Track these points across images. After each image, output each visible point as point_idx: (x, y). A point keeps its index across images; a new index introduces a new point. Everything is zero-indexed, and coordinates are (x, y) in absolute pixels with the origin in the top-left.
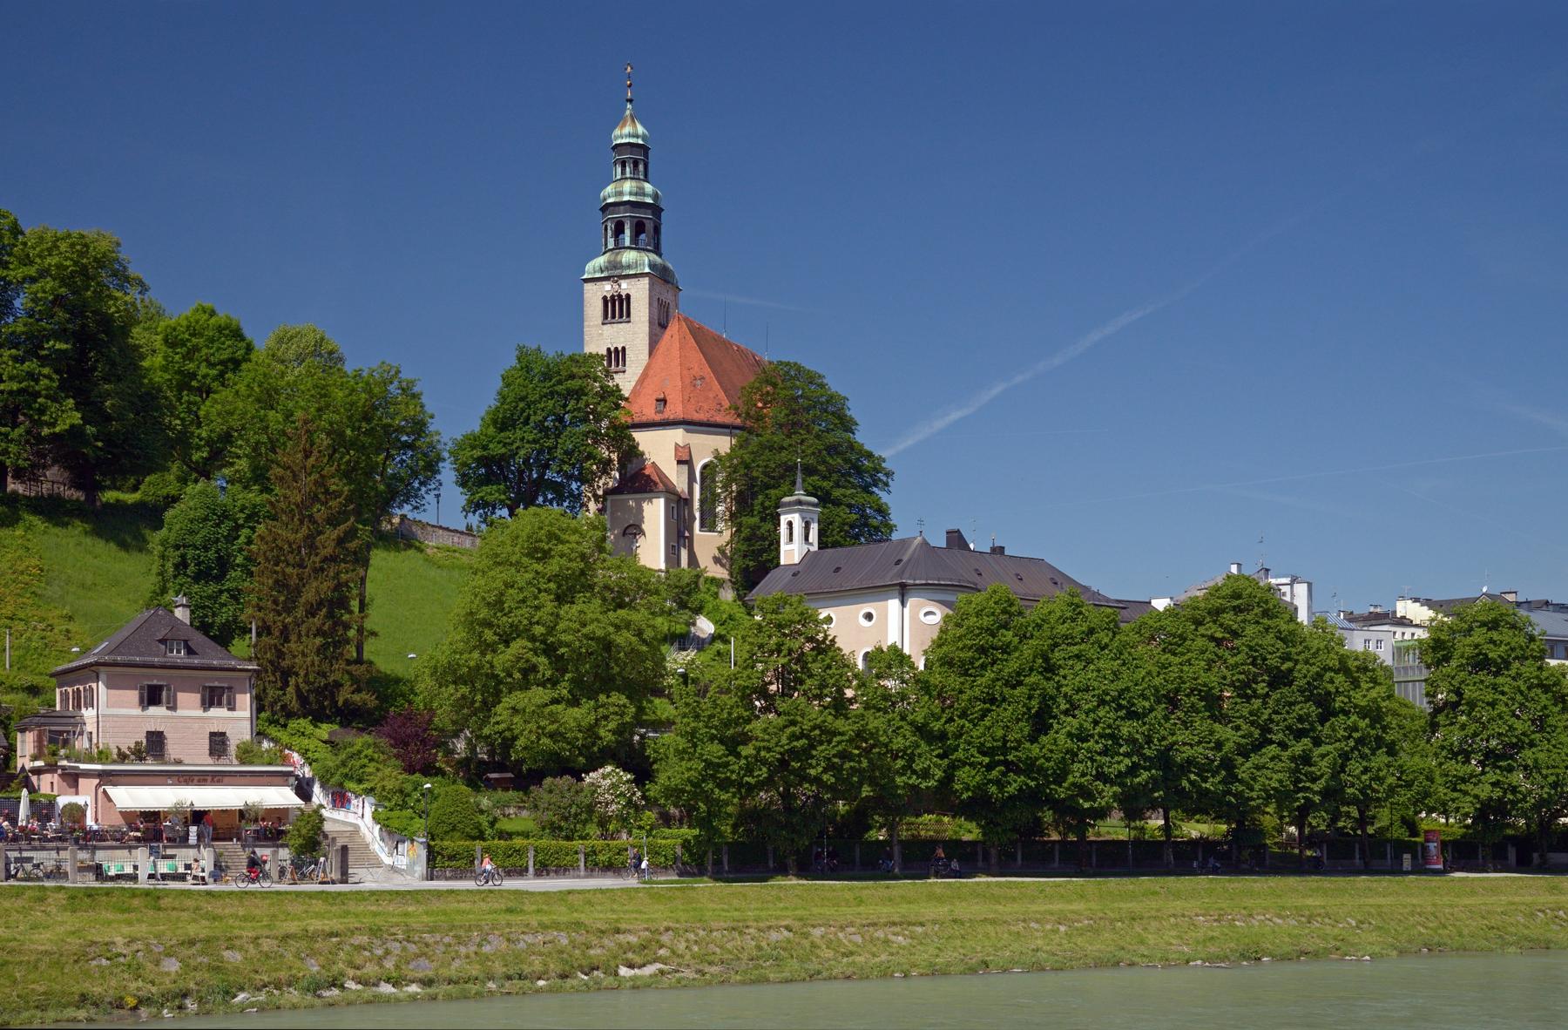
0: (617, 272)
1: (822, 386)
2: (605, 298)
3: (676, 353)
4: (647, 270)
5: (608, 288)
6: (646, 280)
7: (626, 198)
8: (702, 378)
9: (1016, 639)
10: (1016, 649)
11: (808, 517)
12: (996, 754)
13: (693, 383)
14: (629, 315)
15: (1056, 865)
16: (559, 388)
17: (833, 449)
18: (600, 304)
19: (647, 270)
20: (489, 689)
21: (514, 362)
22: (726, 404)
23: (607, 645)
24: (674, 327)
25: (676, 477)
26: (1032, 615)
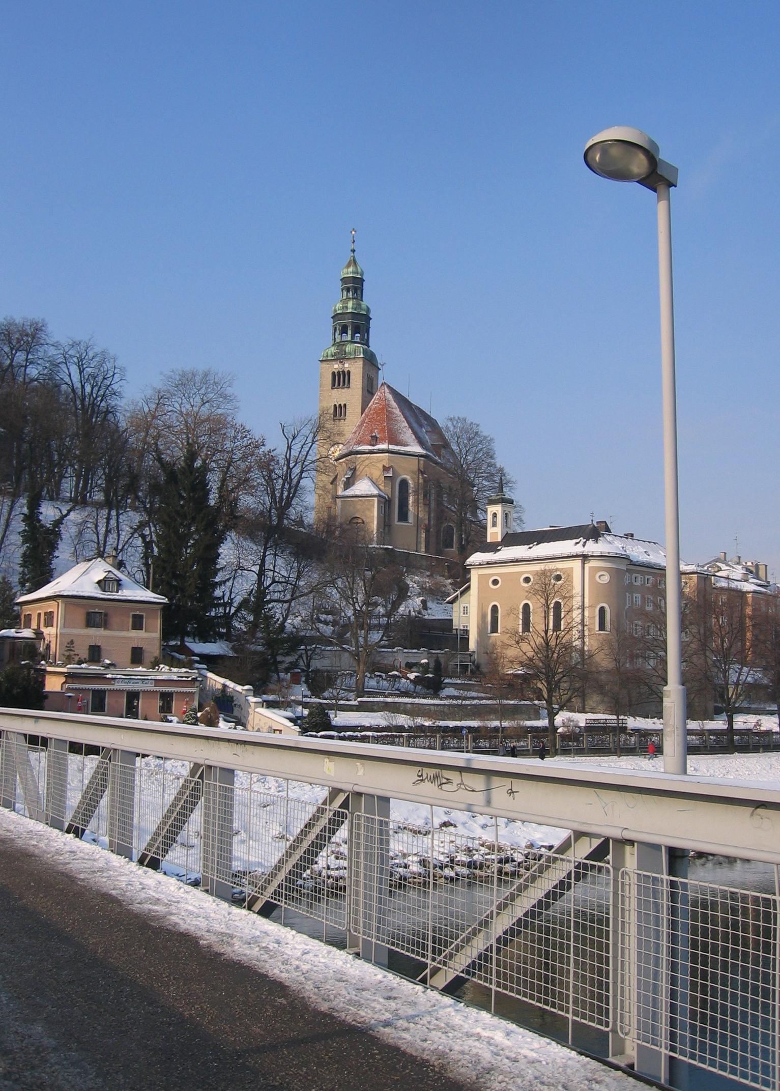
2: (333, 373)
5: (336, 366)
18: (330, 377)
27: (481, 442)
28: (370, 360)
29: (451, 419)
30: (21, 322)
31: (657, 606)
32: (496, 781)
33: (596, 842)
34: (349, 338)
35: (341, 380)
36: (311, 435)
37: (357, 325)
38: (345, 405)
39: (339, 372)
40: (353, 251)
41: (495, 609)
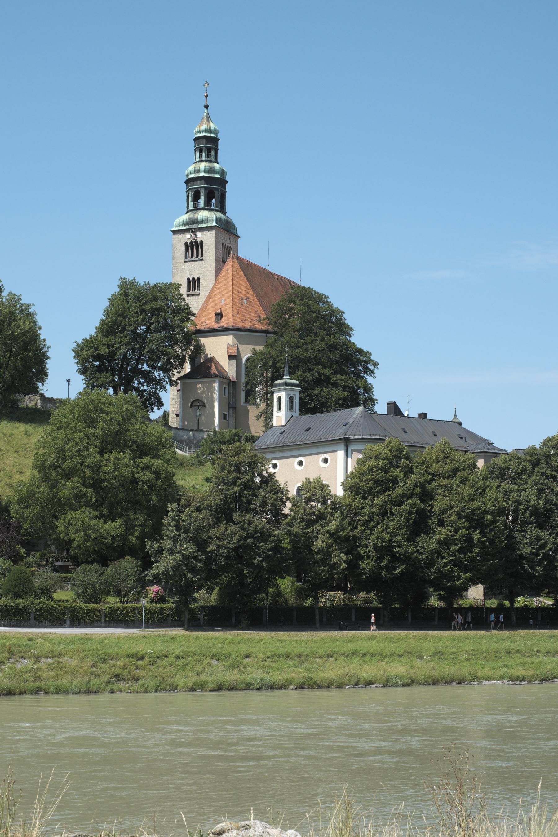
0: (195, 226)
1: (329, 304)
2: (186, 244)
3: (230, 281)
4: (214, 224)
5: (188, 237)
6: (213, 233)
7: (202, 174)
8: (247, 299)
9: (402, 475)
10: (401, 480)
11: (292, 394)
12: (385, 550)
13: (239, 304)
14: (202, 256)
15: (436, 622)
16: (147, 307)
17: (332, 347)
18: (182, 248)
19: (214, 224)
20: (56, 507)
21: (117, 290)
22: (264, 315)
23: (134, 481)
24: (229, 263)
25: (229, 368)
26: (417, 457)
28: (226, 229)
30: (182, 458)
31: (542, 596)
33: (206, 689)
35: (194, 250)
37: (211, 191)
38: (198, 278)
39: (191, 243)
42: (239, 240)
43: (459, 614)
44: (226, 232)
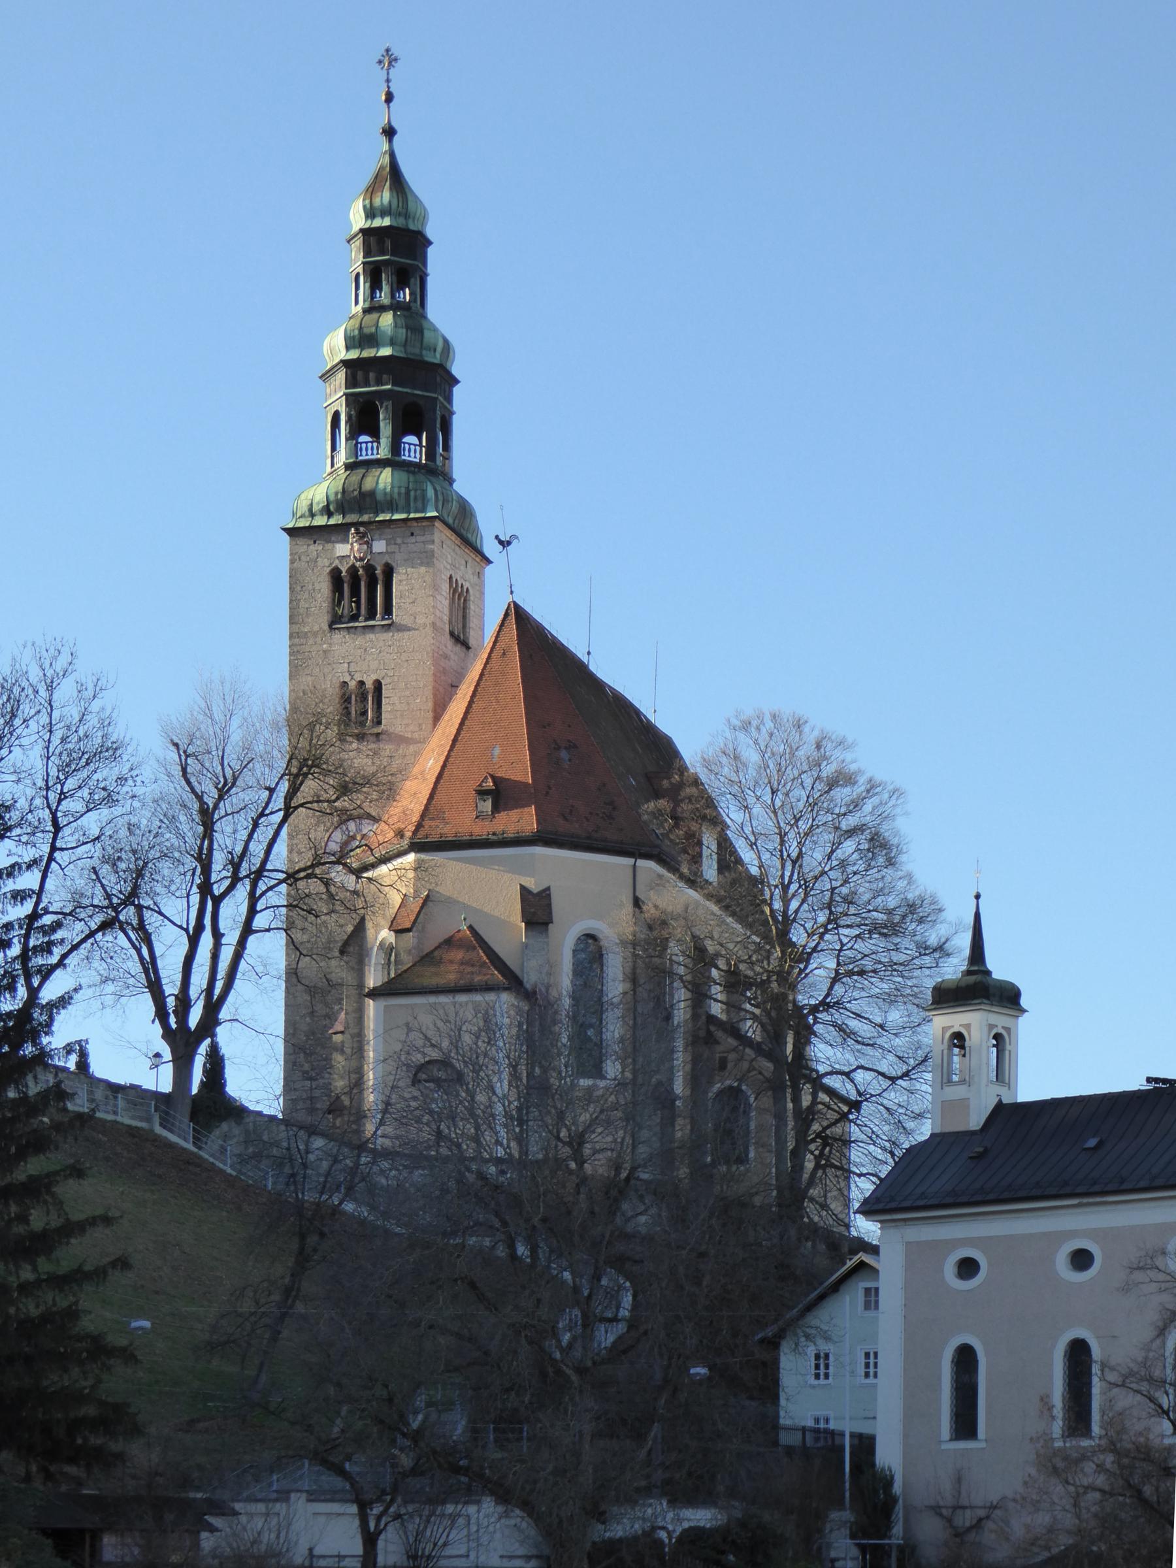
2: (335, 575)
5: (347, 550)
14: (388, 610)
27: (856, 805)
29: (746, 726)
32: (59, 844)
34: (383, 452)
36: (284, 786)
39: (353, 570)
40: (389, 132)
41: (965, 1359)
42: (489, 569)
43: (210, 1519)
44: (458, 541)
